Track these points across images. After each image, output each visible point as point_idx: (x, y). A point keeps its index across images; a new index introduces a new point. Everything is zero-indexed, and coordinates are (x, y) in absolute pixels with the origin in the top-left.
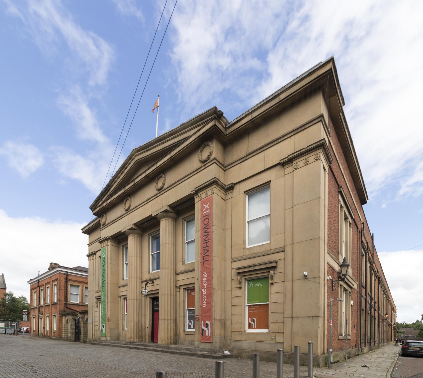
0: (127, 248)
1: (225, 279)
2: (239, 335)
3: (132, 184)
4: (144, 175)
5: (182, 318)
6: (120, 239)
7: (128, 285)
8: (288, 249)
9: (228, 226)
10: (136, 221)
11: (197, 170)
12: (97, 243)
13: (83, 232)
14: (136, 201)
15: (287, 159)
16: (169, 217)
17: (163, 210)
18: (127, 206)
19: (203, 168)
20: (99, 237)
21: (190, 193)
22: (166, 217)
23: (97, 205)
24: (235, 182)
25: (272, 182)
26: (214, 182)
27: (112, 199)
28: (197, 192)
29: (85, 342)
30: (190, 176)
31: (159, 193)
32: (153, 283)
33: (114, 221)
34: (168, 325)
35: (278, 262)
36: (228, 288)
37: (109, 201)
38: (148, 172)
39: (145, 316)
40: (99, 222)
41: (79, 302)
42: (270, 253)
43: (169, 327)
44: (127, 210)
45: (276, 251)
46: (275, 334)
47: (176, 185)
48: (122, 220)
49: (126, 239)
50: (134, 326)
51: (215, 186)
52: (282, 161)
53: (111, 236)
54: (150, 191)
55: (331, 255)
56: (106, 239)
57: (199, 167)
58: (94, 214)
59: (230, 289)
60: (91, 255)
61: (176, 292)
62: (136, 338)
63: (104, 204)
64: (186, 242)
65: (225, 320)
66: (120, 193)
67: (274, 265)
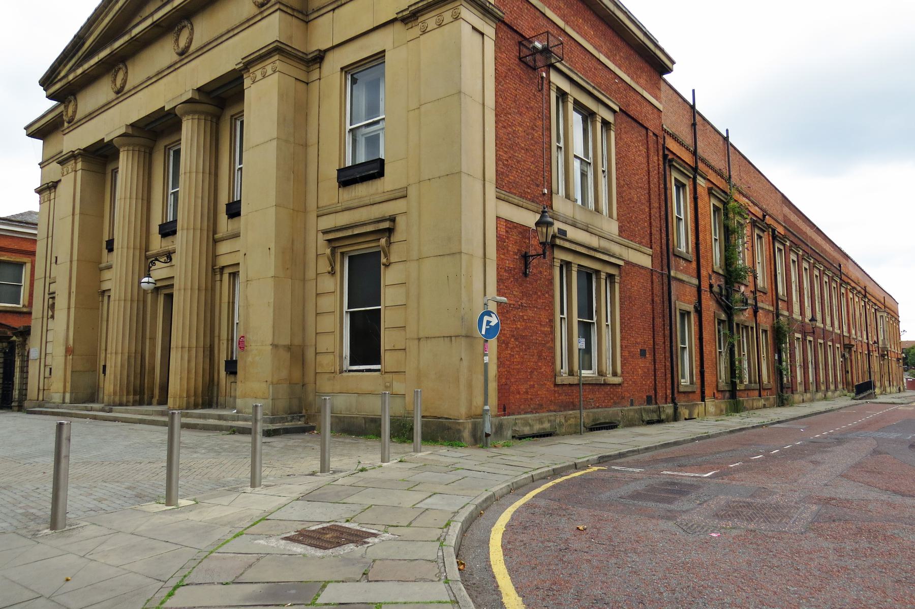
0: (177, 153)
1: (305, 254)
2: (329, 379)
3: (126, 38)
4: (149, 22)
5: (225, 342)
6: (100, 156)
7: (114, 266)
8: (412, 192)
9: (313, 139)
10: (134, 118)
11: (248, 20)
12: (54, 165)
13: (28, 135)
14: (138, 71)
15: (407, 12)
16: (200, 113)
17: (184, 98)
18: (183, 43)
19: (259, 18)
20: (58, 151)
21: (234, 67)
22: (194, 112)
23: (56, 77)
24: (324, 47)
25: (387, 54)
26: (278, 50)
27: (86, 66)
28: (249, 64)
29: (20, 408)
30: (236, 32)
31: (181, 61)
32: (171, 260)
33: (90, 114)
34: (189, 361)
35: (397, 219)
36: (311, 274)
37: (79, 71)
38: (157, 16)
39: (153, 339)
40: (60, 115)
41: (21, 306)
42: (378, 199)
43: (193, 364)
44: (118, 92)
45: (392, 196)
46: (391, 375)
47: (211, 46)
48: (107, 118)
49: (115, 156)
50: (122, 366)
51: (277, 57)
52: (400, 15)
53: (84, 150)
54: (163, 54)
55: (516, 201)
56: (73, 156)
57: (110, 99)
58: (50, 97)
59: (314, 276)
60: (47, 189)
61: (214, 281)
62: (128, 394)
63: (71, 77)
64: (349, 127)
65: (303, 349)
66: (103, 54)
67: (386, 225)
